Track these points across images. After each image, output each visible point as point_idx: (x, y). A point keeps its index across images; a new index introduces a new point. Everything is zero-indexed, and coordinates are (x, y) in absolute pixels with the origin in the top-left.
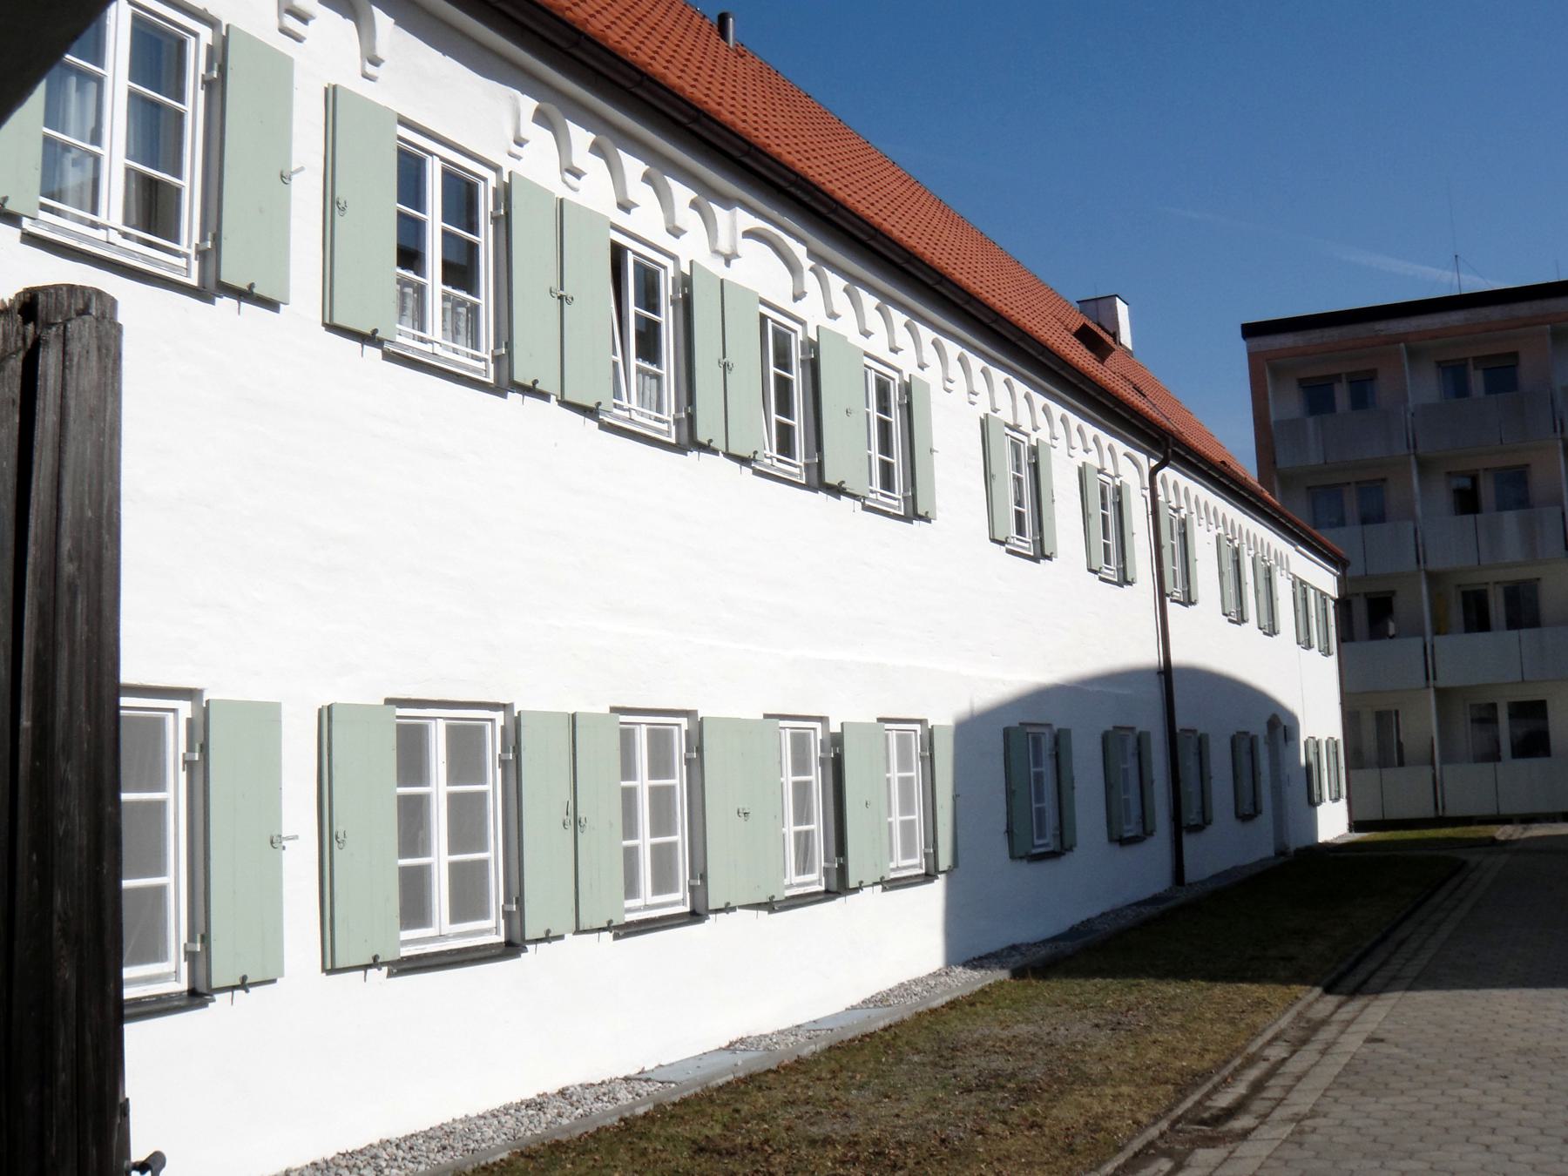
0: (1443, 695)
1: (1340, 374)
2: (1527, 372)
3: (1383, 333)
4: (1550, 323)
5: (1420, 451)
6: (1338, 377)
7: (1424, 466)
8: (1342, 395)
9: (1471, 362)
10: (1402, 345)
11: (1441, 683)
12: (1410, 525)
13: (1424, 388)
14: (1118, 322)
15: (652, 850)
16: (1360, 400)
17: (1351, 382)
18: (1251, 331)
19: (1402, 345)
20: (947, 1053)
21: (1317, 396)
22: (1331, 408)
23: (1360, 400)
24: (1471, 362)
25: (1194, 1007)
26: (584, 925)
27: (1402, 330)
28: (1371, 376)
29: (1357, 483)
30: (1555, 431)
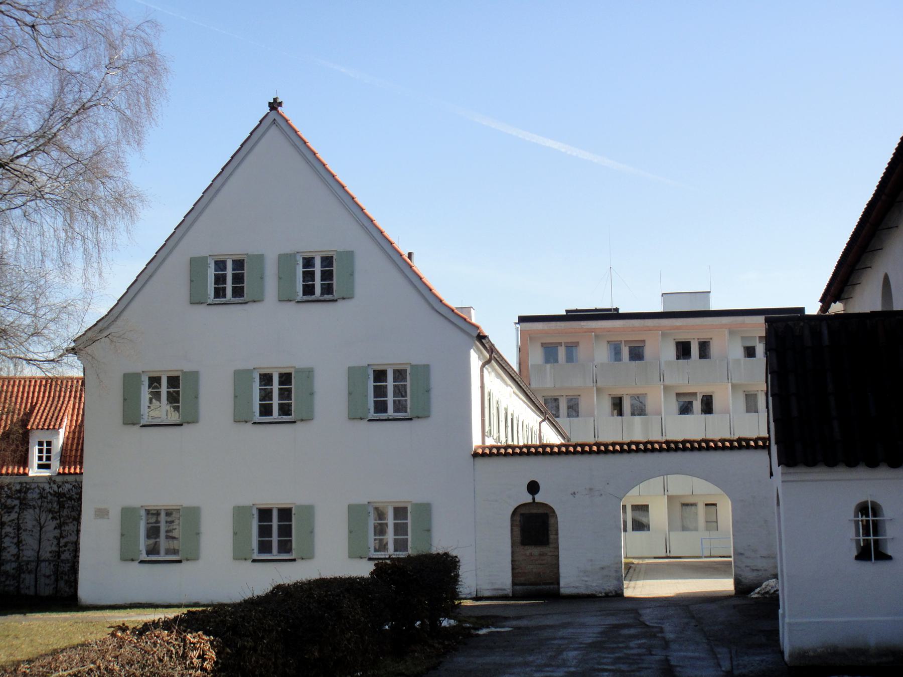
0: (671, 499)
1: (562, 343)
2: (648, 352)
3: (585, 327)
4: (661, 330)
5: (599, 384)
6: (560, 344)
7: (599, 390)
8: (562, 352)
9: (623, 342)
10: (593, 333)
11: (670, 493)
12: (593, 419)
13: (602, 354)
14: (597, 320)
15: (407, 518)
16: (570, 358)
17: (567, 347)
18: (523, 319)
19: (593, 333)
20: (636, 611)
21: (550, 351)
22: (556, 361)
23: (570, 358)
24: (623, 342)
25: (495, 643)
26: (715, 520)
27: (594, 327)
28: (576, 344)
29: (566, 396)
30: (660, 381)
